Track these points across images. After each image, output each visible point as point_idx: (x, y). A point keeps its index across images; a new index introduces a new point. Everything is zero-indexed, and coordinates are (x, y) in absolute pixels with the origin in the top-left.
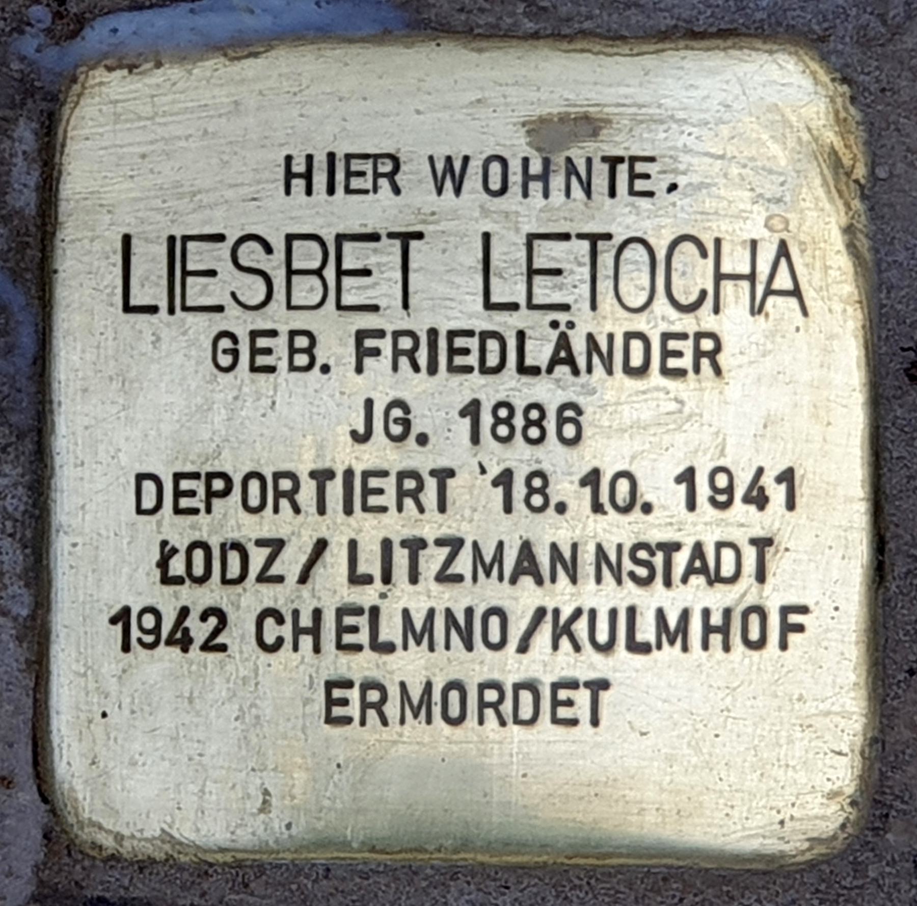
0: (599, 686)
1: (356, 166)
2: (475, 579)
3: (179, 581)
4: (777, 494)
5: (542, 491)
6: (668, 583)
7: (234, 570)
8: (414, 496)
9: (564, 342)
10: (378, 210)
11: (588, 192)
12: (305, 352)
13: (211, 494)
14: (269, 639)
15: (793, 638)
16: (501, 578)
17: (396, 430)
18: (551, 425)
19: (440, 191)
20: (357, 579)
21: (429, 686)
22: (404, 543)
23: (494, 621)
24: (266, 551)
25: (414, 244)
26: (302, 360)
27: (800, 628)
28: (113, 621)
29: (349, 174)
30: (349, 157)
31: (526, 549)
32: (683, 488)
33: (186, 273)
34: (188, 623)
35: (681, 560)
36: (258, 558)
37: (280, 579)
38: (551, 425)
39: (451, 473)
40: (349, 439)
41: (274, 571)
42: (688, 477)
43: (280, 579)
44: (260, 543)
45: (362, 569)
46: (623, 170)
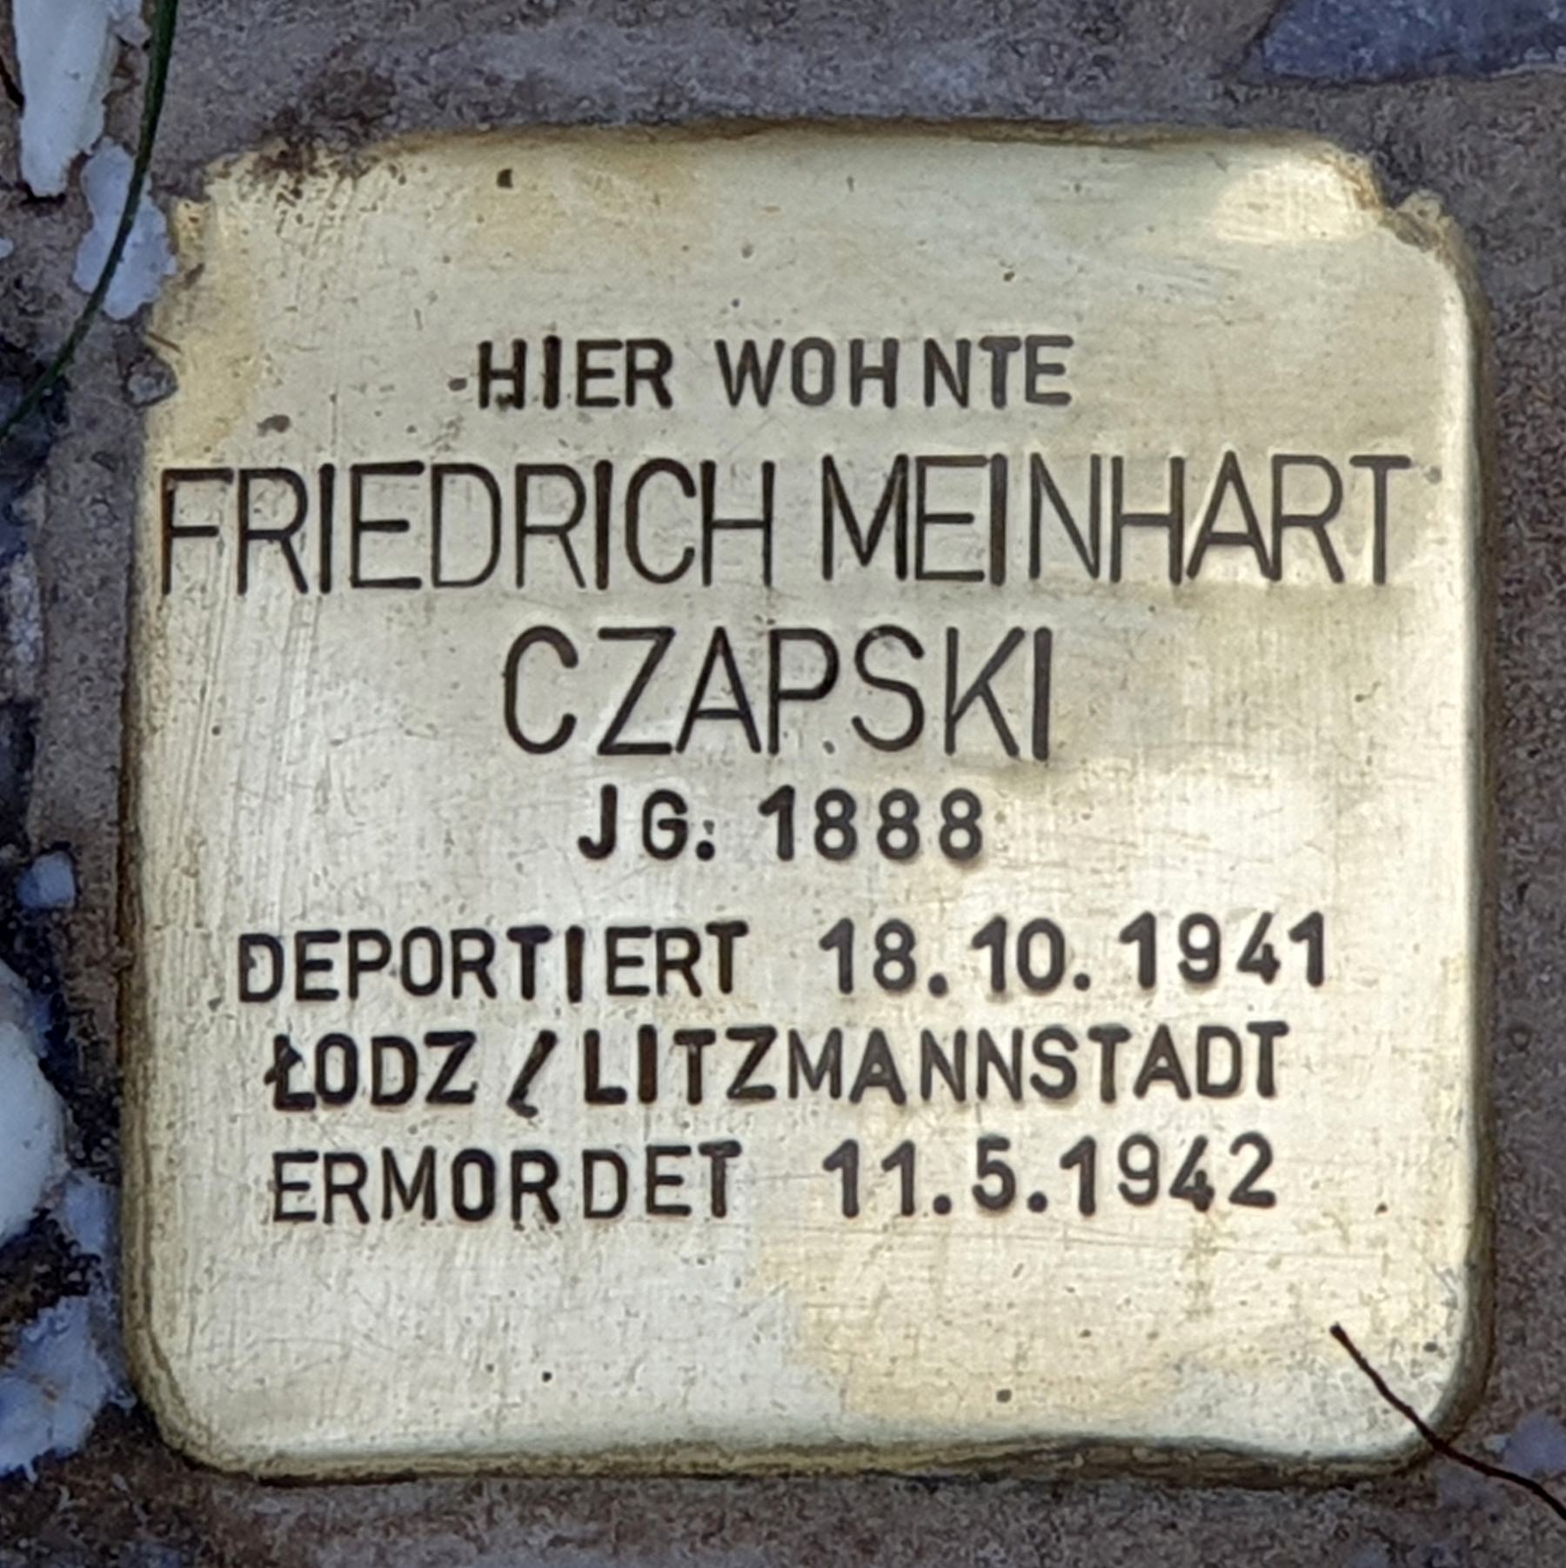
0: (722, 1153)
1: (596, 359)
2: (793, 1092)
4: (1293, 957)
6: (1109, 1095)
7: (393, 1081)
10: (630, 435)
11: (963, 400)
13: (357, 967)
16: (836, 1092)
17: (663, 839)
19: (734, 399)
20: (597, 1094)
21: (429, 1156)
29: (585, 373)
30: (584, 347)
32: (1133, 949)
33: (924, 519)
36: (432, 1062)
37: (466, 1097)
41: (459, 1083)
42: (1142, 931)
44: (434, 1039)
45: (607, 1080)
46: (1017, 363)
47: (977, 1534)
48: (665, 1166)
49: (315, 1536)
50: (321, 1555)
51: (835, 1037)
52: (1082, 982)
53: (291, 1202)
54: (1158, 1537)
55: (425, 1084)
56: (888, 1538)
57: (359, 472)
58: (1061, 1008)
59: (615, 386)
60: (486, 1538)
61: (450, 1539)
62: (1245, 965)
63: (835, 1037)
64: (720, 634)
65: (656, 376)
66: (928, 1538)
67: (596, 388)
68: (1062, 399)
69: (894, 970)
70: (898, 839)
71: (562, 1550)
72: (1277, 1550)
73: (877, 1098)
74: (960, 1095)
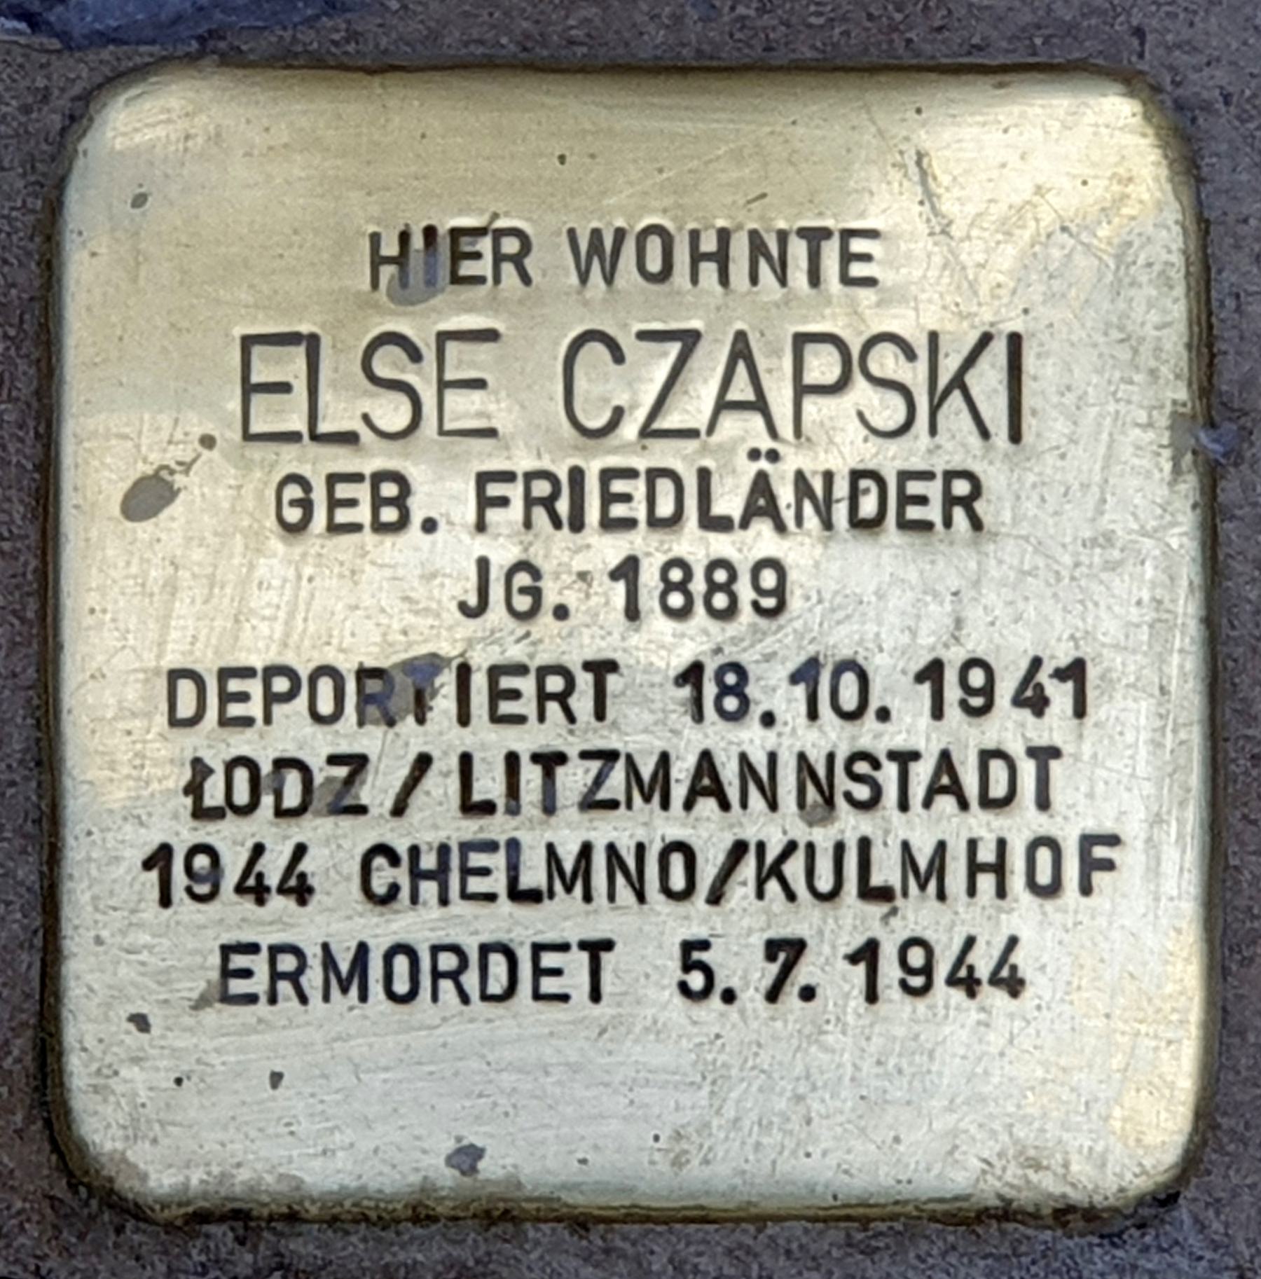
0: (597, 949)
5: (738, 691)
6: (904, 806)
9: (761, 484)
11: (783, 281)
12: (394, 505)
13: (270, 699)
15: (1098, 878)
17: (522, 603)
18: (698, 586)
19: (584, 277)
20: (472, 807)
21: (363, 949)
22: (536, 758)
23: (677, 861)
26: (389, 515)
27: (1109, 865)
28: (148, 865)
35: (921, 773)
38: (698, 586)
39: (608, 945)
40: (458, 615)
48: (549, 960)
51: (664, 759)
58: (869, 735)
63: (664, 759)
64: (741, 336)
65: (518, 260)
68: (870, 282)
70: (720, 601)
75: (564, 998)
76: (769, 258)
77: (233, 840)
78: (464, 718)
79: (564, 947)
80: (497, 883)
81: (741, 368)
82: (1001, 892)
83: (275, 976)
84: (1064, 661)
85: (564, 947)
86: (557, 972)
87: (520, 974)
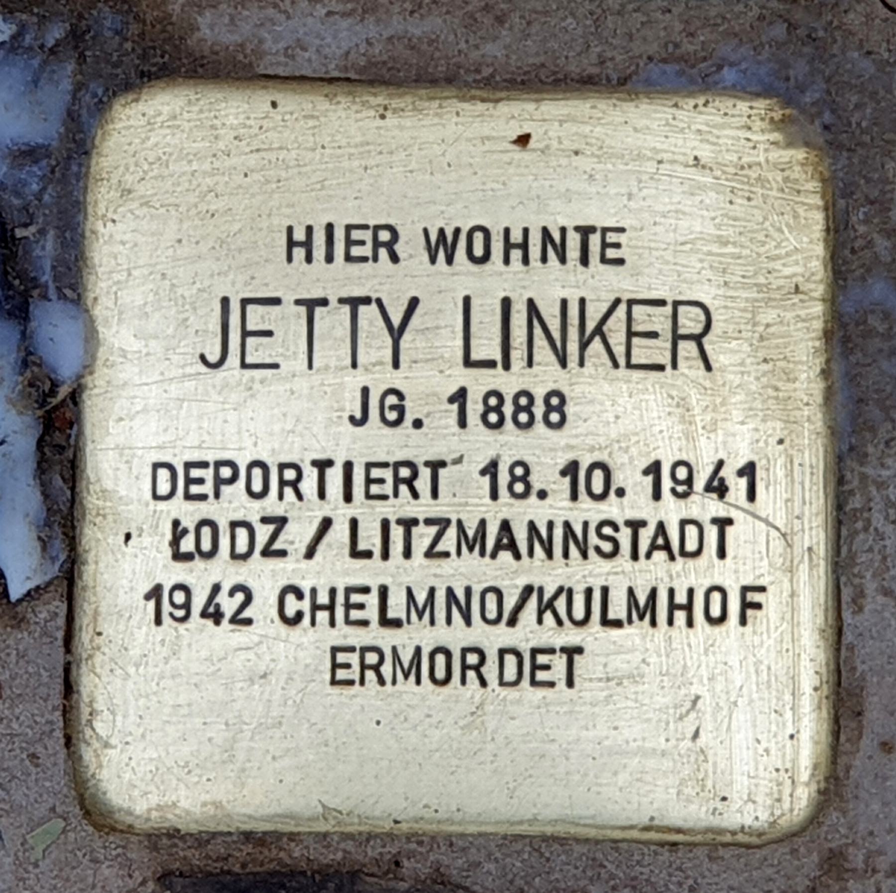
0: (572, 652)
1: (356, 235)
2: (459, 553)
3: (188, 557)
4: (738, 487)
5: (524, 479)
6: (635, 556)
7: (242, 545)
8: (409, 483)
13: (219, 482)
14: (290, 612)
15: (750, 612)
16: (482, 553)
17: (392, 416)
19: (433, 260)
21: (418, 650)
24: (271, 528)
25: (319, 311)
27: (758, 606)
31: (506, 526)
32: (650, 479)
34: (218, 599)
36: (263, 533)
37: (283, 553)
39: (579, 650)
41: (277, 546)
42: (654, 469)
43: (283, 553)
44: (265, 520)
46: (595, 240)
47: (561, 13)
49: (196, 9)
50: (199, 19)
52: (621, 493)
53: (341, 674)
54: (661, 17)
55: (259, 546)
56: (512, 14)
57: (245, 302)
58: (612, 509)
59: (366, 250)
60: (290, 11)
61: (271, 11)
62: (709, 488)
65: (389, 247)
66: (534, 16)
67: (356, 251)
68: (620, 262)
69: (519, 487)
71: (331, 19)
72: (726, 26)
73: (506, 556)
74: (550, 554)
75: (552, 684)
76: (552, 241)
77: (200, 577)
78: (348, 497)
79: (551, 651)
80: (372, 613)
81: (396, 320)
82: (690, 623)
83: (363, 667)
84: (741, 463)
85: (551, 651)
86: (547, 667)
87: (531, 666)
